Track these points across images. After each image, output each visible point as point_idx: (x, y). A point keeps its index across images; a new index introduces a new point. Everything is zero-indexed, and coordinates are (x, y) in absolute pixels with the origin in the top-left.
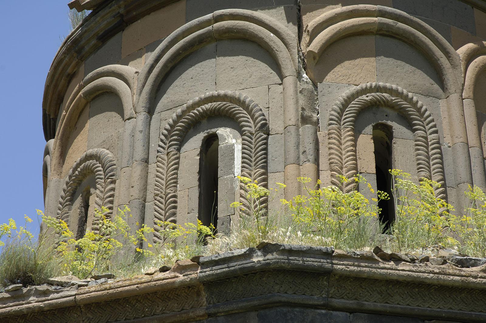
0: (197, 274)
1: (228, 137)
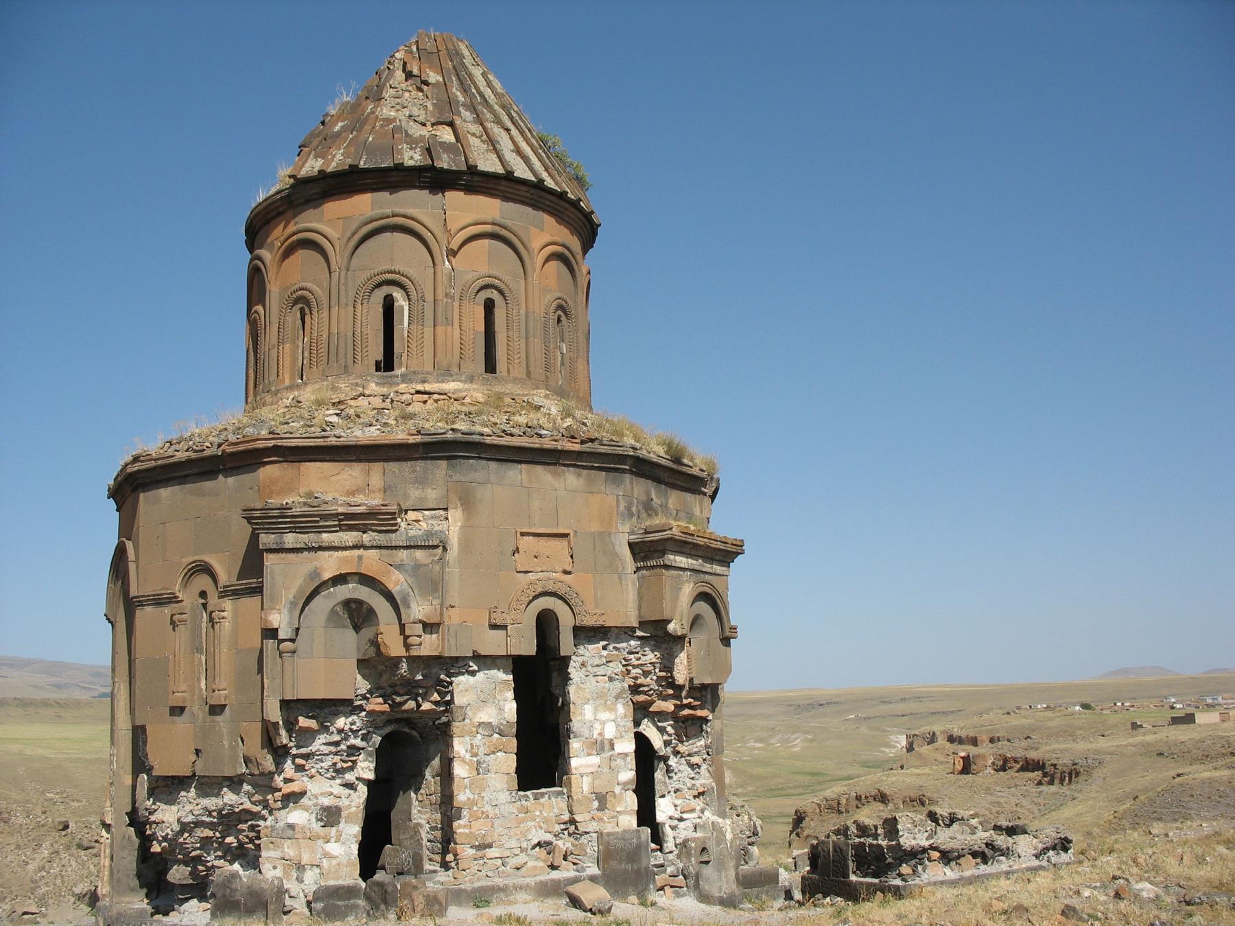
0: (418, 439)
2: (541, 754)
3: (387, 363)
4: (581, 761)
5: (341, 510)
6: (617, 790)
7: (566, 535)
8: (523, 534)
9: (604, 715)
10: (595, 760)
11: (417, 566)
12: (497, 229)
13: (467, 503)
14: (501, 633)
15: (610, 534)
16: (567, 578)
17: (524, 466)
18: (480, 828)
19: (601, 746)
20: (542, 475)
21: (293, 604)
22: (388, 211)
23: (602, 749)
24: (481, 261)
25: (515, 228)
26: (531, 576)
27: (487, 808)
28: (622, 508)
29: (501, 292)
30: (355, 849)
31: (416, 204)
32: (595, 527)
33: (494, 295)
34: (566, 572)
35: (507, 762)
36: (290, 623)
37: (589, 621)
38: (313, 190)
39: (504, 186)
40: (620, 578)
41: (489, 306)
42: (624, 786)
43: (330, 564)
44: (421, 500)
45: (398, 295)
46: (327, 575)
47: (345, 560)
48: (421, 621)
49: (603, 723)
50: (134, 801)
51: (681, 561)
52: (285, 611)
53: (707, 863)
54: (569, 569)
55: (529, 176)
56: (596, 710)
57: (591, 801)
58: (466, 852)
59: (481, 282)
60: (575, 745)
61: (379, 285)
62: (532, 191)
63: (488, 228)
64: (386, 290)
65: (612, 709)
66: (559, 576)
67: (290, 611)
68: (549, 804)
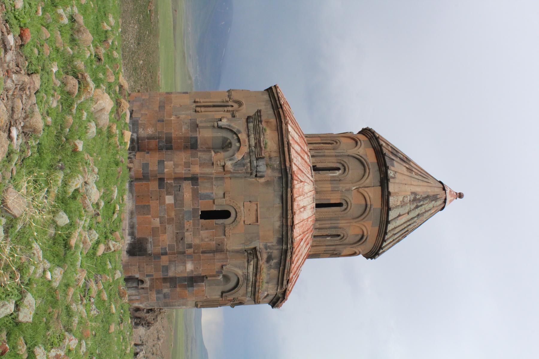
1: (337, 173)
5: (262, 139)
7: (257, 221)
8: (257, 204)
12: (369, 206)
14: (222, 196)
15: (259, 239)
16: (242, 223)
17: (281, 205)
20: (278, 213)
21: (230, 126)
22: (370, 167)
24: (355, 201)
25: (370, 214)
26: (242, 208)
28: (269, 244)
29: (346, 209)
31: (373, 177)
32: (261, 234)
33: (344, 206)
34: (244, 222)
36: (223, 125)
38: (376, 145)
39: (385, 208)
40: (243, 244)
41: (340, 205)
43: (243, 136)
45: (340, 171)
46: (239, 135)
47: (245, 141)
48: (225, 164)
50: (133, 287)
51: (251, 268)
52: (227, 123)
53: (136, 345)
54: (246, 223)
55: (384, 245)
59: (348, 201)
61: (343, 166)
62: (385, 220)
63: (369, 203)
64: (342, 168)
66: (243, 219)
67: (227, 125)
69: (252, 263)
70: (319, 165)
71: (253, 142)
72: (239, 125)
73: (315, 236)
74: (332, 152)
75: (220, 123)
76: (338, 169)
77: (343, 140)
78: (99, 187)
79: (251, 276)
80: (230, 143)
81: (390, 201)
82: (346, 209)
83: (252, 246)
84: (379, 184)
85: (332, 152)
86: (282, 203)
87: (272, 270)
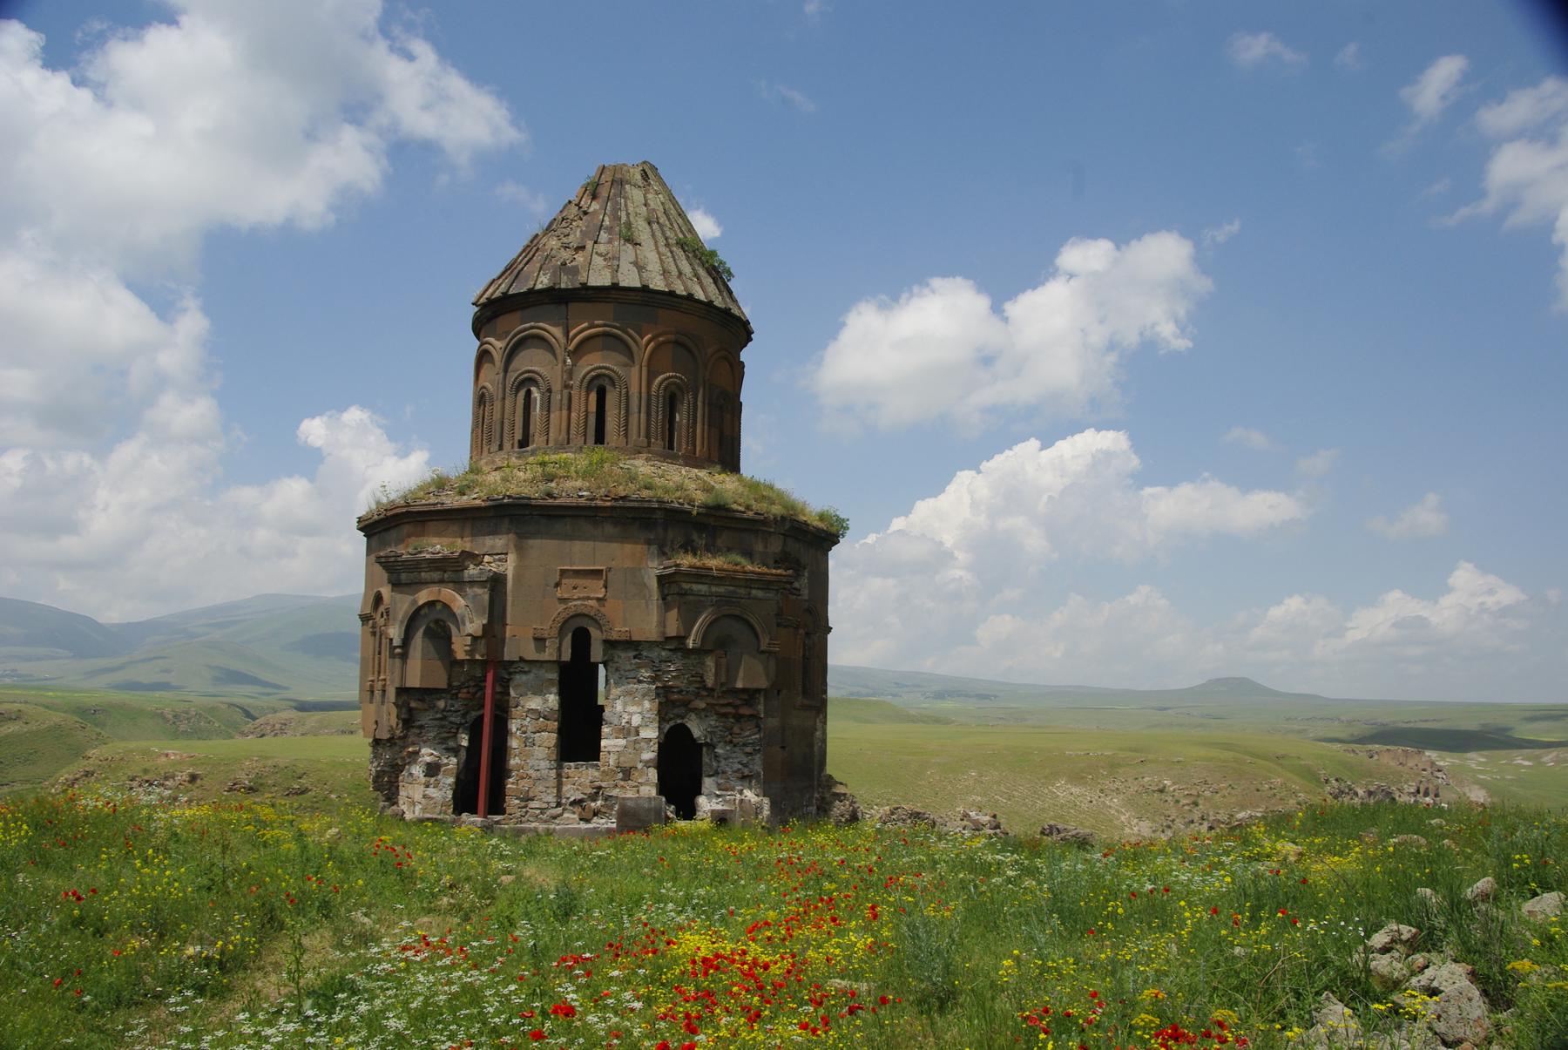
1: (536, 394)
2: (579, 735)
3: (524, 443)
4: (610, 743)
6: (640, 766)
9: (631, 709)
10: (622, 742)
11: (475, 596)
13: (520, 550)
18: (524, 785)
19: (626, 731)
23: (629, 734)
27: (531, 772)
30: (450, 794)
35: (549, 738)
37: (614, 636)
42: (647, 764)
43: (423, 596)
44: (493, 547)
45: (533, 389)
49: (631, 714)
55: (702, 298)
56: (625, 704)
57: (616, 773)
58: (512, 803)
60: (605, 730)
64: (596, 382)
65: (640, 704)
68: (581, 777)
69: (686, 586)
70: (518, 435)
71: (436, 575)
72: (402, 605)
73: (501, 448)
74: (498, 405)
75: (395, 643)
76: (529, 393)
77: (482, 382)
78: (809, 611)
79: (721, 589)
80: (437, 622)
81: (599, 284)
82: (611, 379)
83: (654, 584)
84: (563, 307)
85: (498, 405)
86: (564, 516)
87: (719, 542)
